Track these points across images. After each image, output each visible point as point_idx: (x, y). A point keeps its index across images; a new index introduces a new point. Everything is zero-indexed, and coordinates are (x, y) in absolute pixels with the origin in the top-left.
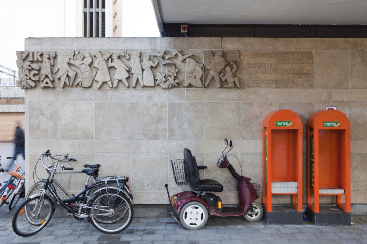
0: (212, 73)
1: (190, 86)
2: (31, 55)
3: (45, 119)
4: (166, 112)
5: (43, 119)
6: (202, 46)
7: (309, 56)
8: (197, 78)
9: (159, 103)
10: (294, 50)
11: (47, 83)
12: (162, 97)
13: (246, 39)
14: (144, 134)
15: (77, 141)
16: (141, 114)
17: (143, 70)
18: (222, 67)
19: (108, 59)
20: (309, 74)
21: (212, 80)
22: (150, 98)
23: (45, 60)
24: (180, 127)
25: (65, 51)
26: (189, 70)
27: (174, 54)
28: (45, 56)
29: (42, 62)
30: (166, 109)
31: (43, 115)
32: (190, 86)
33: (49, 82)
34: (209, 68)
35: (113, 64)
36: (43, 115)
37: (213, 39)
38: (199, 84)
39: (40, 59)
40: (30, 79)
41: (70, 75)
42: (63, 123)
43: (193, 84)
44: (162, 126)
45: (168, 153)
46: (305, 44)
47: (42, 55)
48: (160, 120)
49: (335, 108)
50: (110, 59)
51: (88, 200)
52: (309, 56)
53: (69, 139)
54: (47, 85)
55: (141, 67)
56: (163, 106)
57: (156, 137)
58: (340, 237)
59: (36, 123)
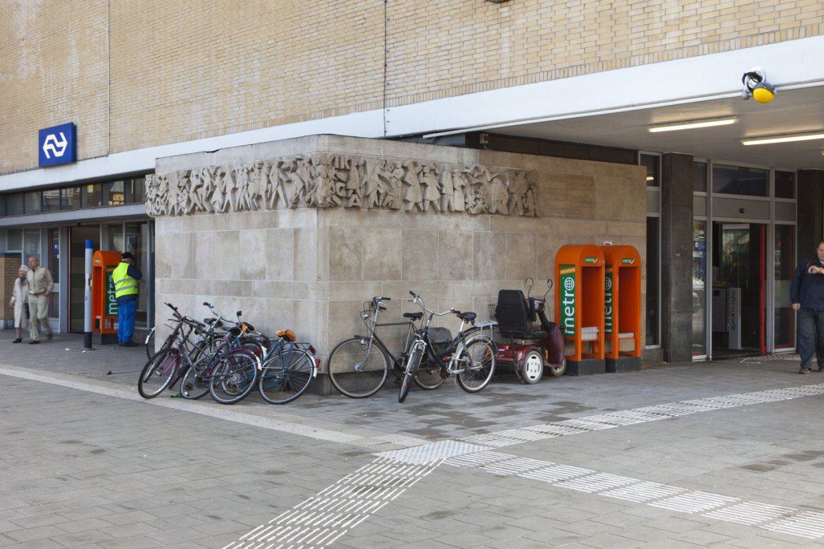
0: (516, 197)
1: (497, 212)
2: (337, 160)
3: (348, 251)
4: (471, 245)
5: (345, 251)
6: (505, 161)
7: (589, 182)
8: (503, 202)
9: (466, 233)
10: (581, 174)
11: (355, 201)
12: (469, 225)
13: (542, 158)
14: (451, 273)
15: (382, 282)
16: (449, 247)
17: (454, 189)
18: (524, 191)
19: (419, 173)
20: (591, 203)
21: (312, 137)
22: (457, 226)
23: (353, 168)
24: (485, 264)
25: (371, 158)
26: (496, 190)
27: (482, 171)
28: (354, 163)
29: (349, 170)
30: (472, 241)
31: (346, 245)
32: (497, 212)
33: (358, 200)
34: (513, 191)
35: (426, 180)
36: (346, 245)
37: (514, 154)
38: (505, 211)
39: (348, 167)
40: (336, 194)
41: (382, 191)
42: (368, 257)
43: (500, 210)
44: (468, 262)
45: (473, 298)
46: (588, 167)
47: (349, 162)
48: (466, 255)
49: (611, 243)
50: (422, 173)
51: (564, 363)
52: (589, 182)
53: (374, 279)
54: (355, 204)
55: (452, 185)
56: (469, 237)
57: (462, 277)
58: (112, 456)
59: (337, 257)
